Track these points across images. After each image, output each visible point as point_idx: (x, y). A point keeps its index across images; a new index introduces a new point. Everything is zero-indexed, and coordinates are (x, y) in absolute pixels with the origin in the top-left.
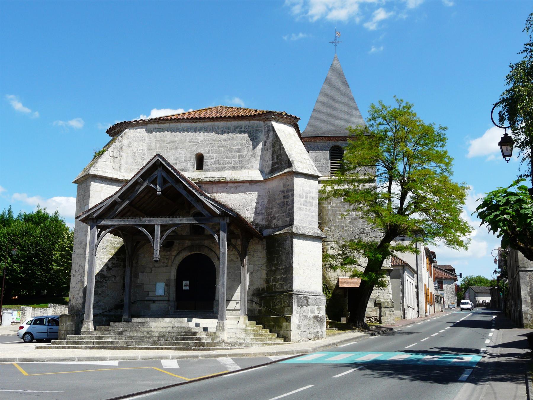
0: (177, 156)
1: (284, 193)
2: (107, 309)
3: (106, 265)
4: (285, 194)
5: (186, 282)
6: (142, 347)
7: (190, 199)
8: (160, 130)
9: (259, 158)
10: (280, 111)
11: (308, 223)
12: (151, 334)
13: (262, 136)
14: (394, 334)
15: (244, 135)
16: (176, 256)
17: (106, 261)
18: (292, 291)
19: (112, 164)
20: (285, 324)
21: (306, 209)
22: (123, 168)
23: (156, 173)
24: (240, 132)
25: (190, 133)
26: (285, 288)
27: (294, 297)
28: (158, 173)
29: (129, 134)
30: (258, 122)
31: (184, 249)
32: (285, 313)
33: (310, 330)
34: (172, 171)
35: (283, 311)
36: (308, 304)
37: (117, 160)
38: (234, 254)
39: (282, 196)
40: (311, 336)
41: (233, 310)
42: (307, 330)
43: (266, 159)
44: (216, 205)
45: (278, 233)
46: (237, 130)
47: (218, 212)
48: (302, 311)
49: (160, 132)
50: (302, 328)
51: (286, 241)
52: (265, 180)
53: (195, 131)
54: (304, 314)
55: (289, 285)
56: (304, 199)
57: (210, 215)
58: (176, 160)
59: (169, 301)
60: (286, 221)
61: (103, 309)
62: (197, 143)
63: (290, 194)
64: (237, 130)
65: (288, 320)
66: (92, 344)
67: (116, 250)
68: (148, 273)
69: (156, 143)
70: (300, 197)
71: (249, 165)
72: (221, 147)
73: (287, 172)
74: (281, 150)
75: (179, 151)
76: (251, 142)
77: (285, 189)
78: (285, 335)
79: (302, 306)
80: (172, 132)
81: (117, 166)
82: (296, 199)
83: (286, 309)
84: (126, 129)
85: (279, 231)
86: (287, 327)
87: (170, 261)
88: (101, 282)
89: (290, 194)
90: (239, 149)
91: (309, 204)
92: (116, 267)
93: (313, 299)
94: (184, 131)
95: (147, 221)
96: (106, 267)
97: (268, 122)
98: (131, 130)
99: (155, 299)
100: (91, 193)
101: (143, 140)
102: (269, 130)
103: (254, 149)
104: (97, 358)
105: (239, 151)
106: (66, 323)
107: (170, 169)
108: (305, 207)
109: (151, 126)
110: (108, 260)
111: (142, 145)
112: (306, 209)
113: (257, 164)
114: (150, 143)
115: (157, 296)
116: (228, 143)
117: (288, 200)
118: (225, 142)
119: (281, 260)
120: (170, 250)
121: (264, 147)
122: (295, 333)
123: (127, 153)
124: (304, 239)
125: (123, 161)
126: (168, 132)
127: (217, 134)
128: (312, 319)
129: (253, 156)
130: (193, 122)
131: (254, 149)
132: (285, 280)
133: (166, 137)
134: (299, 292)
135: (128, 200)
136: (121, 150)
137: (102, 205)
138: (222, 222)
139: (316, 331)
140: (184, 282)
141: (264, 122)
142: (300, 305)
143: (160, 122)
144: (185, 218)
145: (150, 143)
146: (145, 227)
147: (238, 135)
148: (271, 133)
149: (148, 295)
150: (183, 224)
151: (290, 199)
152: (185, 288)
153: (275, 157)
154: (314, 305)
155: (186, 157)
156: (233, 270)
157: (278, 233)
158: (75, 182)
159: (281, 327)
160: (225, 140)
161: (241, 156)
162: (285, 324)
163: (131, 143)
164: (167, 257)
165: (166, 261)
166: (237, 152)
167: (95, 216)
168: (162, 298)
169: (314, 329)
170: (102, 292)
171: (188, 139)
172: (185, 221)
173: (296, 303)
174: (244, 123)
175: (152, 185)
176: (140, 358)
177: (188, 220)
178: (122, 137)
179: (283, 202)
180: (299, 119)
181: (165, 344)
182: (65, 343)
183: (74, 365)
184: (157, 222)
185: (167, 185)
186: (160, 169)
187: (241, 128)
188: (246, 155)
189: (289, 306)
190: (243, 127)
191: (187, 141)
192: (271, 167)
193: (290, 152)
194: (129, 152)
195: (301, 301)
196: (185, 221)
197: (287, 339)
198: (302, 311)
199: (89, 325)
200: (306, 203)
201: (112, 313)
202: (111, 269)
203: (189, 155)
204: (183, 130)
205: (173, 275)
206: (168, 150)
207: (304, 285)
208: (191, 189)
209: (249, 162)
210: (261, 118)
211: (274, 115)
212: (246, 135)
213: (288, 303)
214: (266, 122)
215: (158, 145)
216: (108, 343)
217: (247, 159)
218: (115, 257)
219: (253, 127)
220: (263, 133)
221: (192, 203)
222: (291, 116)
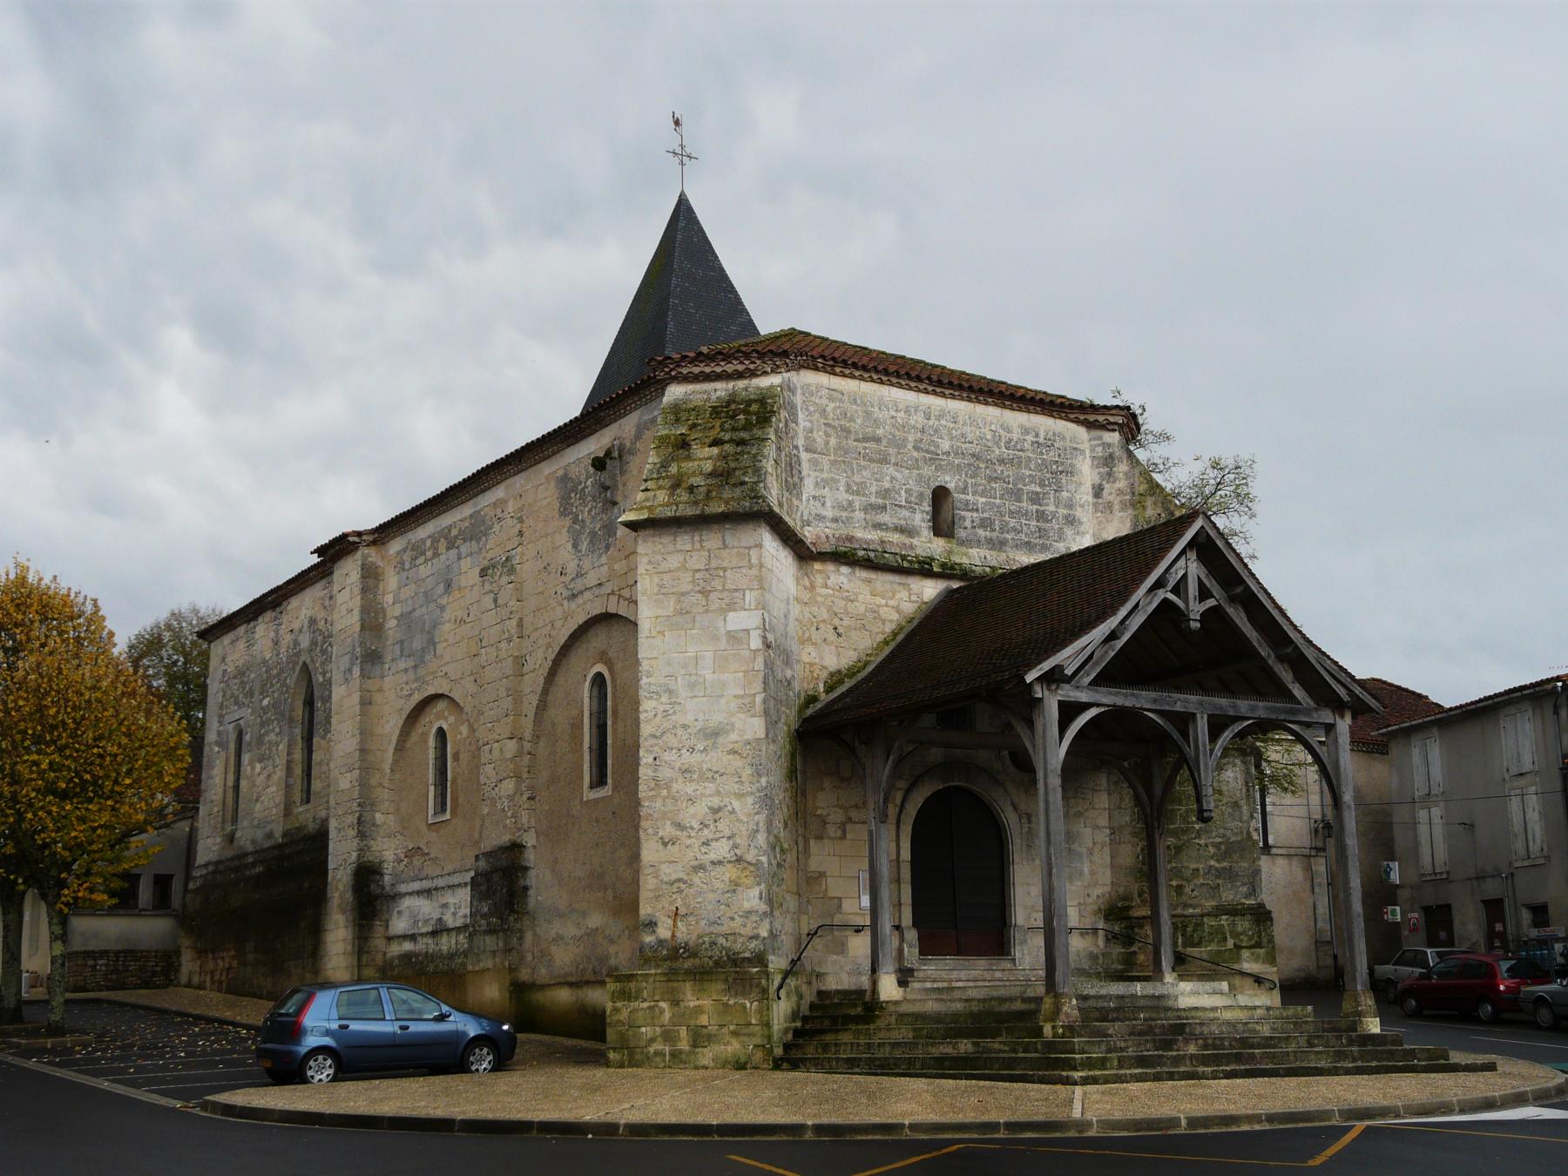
0: (887, 485)
69: (827, 435)
72: (996, 479)
105: (1036, 499)
106: (676, 1003)
114: (811, 431)
188: (1054, 514)
191: (910, 446)
213: (1251, 938)
215: (833, 441)
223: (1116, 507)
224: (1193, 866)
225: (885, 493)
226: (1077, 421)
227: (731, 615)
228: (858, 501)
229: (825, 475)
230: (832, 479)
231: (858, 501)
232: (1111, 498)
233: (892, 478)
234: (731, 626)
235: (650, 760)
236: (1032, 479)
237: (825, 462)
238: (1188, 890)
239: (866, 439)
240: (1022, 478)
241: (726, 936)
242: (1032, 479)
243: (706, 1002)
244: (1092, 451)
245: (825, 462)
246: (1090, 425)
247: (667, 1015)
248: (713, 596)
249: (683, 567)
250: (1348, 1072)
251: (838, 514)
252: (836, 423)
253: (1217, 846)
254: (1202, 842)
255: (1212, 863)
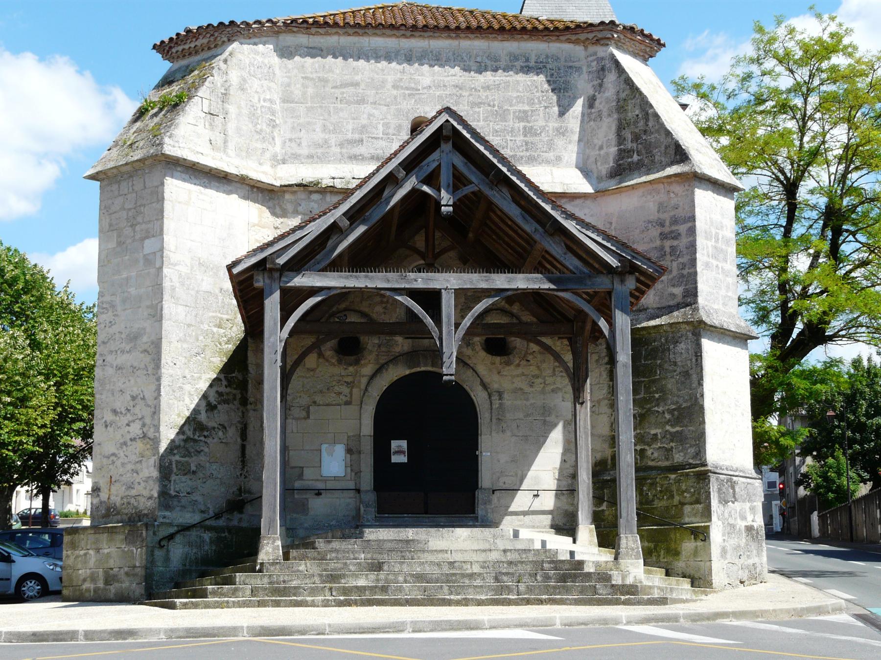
0: (364, 121)
1: (662, 225)
2: (212, 514)
3: (205, 396)
4: (667, 229)
5: (399, 445)
6: (483, 597)
7: (530, 226)
8: (315, 52)
9: (576, 137)
10: (629, 24)
11: (721, 302)
12: (461, 568)
13: (583, 83)
14: (856, 576)
15: (535, 78)
16: (372, 377)
17: (204, 385)
18: (706, 465)
19: (207, 134)
20: (688, 545)
21: (717, 266)
22: (231, 145)
23: (435, 156)
24: (527, 69)
25: (394, 64)
26: (678, 457)
27: (713, 478)
28: (445, 157)
29: (240, 56)
30: (571, 46)
31: (394, 360)
32: (687, 520)
33: (742, 561)
34: (487, 153)
35: (680, 514)
36: (735, 500)
37: (219, 121)
38: (523, 374)
39: (655, 232)
40: (744, 575)
41: (525, 513)
42: (737, 561)
43: (598, 142)
44: (609, 245)
45: (652, 323)
46: (519, 64)
47: (614, 262)
48: (726, 515)
49: (313, 56)
50: (728, 556)
51: (676, 342)
52: (600, 193)
53: (409, 59)
54: (731, 521)
55: (692, 451)
56: (713, 243)
57: (586, 270)
58: (361, 133)
59: (358, 491)
60: (673, 295)
61: (202, 512)
62: (413, 92)
63: (683, 228)
64: (519, 64)
65: (702, 534)
66: (327, 592)
67: (225, 360)
68: (297, 419)
69: (304, 86)
70: (707, 238)
71: (551, 155)
72: (479, 104)
73: (676, 175)
74: (647, 120)
75: (368, 109)
76: (555, 98)
77: (666, 216)
78: (689, 571)
79: (727, 502)
80: (345, 59)
81: (219, 139)
82: (701, 243)
83: (687, 509)
84: (230, 41)
85: (649, 319)
86: (696, 553)
87: (355, 390)
88: (195, 441)
89: (683, 228)
90: (525, 112)
91: (721, 256)
92: (226, 402)
93: (743, 486)
94: (378, 59)
95: (421, 281)
96: (204, 404)
97: (601, 51)
98: (245, 47)
99: (320, 485)
100: (167, 206)
101: (270, 76)
102: (603, 69)
103: (562, 114)
104: (459, 622)
105: (524, 116)
106: (98, 550)
107: (481, 148)
108: (715, 263)
109: (289, 39)
110: (208, 384)
111: (269, 89)
112: (717, 266)
113: (570, 152)
114: (289, 85)
115: (326, 480)
116: (495, 97)
117: (675, 243)
118: (488, 93)
119: (662, 390)
120: (357, 362)
121: (587, 111)
122: (720, 569)
123: (239, 107)
124: (720, 341)
125: (231, 127)
126: (335, 57)
127: (465, 70)
128: (744, 535)
129: (562, 132)
130: (404, 36)
131: (562, 114)
132: (677, 437)
133: (331, 71)
134: (716, 468)
135: (363, 222)
136: (225, 96)
137: (299, 234)
138: (618, 286)
139: (751, 562)
140: (395, 444)
141: (586, 48)
142: (724, 501)
143: (313, 30)
144: (521, 276)
145: (289, 85)
146: (414, 294)
147: (521, 77)
148: (611, 77)
149: (301, 476)
150: (517, 289)
151: (684, 241)
152: (395, 459)
153: (629, 136)
154: (744, 501)
155: (387, 125)
156: (521, 415)
157: (652, 323)
158: (92, 177)
159: (677, 553)
160: (487, 88)
161: (527, 131)
162: (688, 545)
163: (244, 80)
164: (349, 379)
165: (346, 390)
166: (521, 119)
167: (281, 261)
168: (338, 485)
169: (748, 557)
170: (199, 466)
171: (390, 79)
172: (522, 282)
173: (716, 495)
174: (535, 47)
175: (425, 188)
176: (558, 622)
177: (528, 280)
178: (225, 61)
179: (662, 248)
180: (664, 45)
181: (530, 590)
182: (248, 592)
183: (388, 639)
184: (448, 282)
185: (467, 190)
186: (447, 147)
187: (527, 60)
188: (543, 128)
189: (698, 502)
190: (533, 59)
191: (389, 86)
192: (616, 161)
193: (673, 127)
194: (243, 104)
195: (724, 490)
196: (522, 282)
197: (700, 580)
198: (726, 515)
199: (270, 548)
200: (718, 253)
201: (221, 522)
202: (215, 407)
203: (394, 122)
204: (376, 55)
205: (368, 428)
206: (339, 106)
207: (724, 452)
208: (539, 201)
209: (550, 146)
210: (582, 36)
211: (617, 32)
212: (542, 78)
213: (693, 495)
214: (592, 49)
215: (310, 91)
216: (361, 590)
217: (544, 138)
218: (222, 376)
219: (557, 59)
220: (585, 76)
221: (537, 237)
222: (649, 37)
223: (605, 114)
224: (653, 432)
225: (363, 129)
226: (569, 41)
227: (147, 242)
228: (333, 139)
229: (302, 120)
230: (309, 123)
231: (333, 139)
232: (601, 107)
233: (370, 115)
234: (147, 250)
235: (101, 362)
236: (520, 100)
237: (302, 109)
238: (649, 452)
239: (344, 85)
240: (509, 101)
241: (135, 497)
242: (520, 100)
243: (113, 550)
244: (589, 66)
245: (302, 109)
246: (585, 43)
247: (93, 560)
248: (138, 228)
249: (123, 208)
250: (356, 603)
251: (313, 151)
252: (314, 76)
253: (671, 412)
254: (660, 409)
255: (668, 428)
